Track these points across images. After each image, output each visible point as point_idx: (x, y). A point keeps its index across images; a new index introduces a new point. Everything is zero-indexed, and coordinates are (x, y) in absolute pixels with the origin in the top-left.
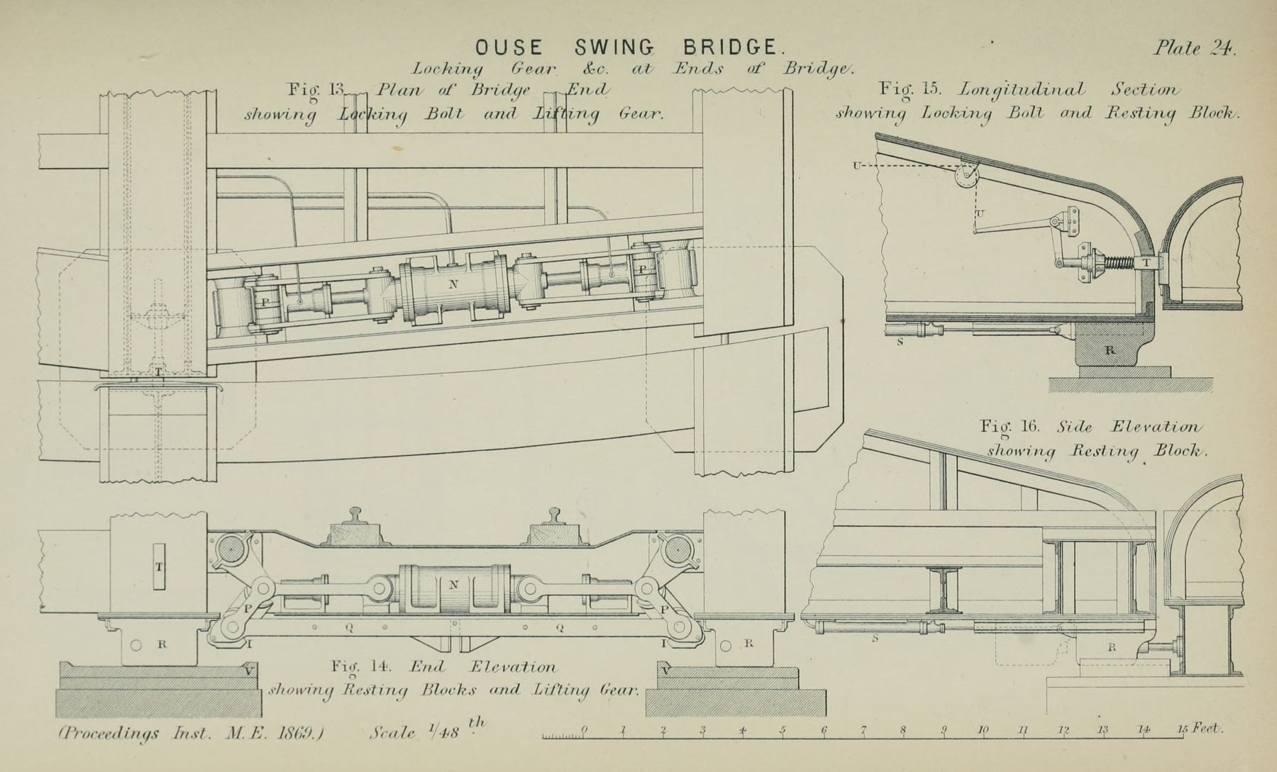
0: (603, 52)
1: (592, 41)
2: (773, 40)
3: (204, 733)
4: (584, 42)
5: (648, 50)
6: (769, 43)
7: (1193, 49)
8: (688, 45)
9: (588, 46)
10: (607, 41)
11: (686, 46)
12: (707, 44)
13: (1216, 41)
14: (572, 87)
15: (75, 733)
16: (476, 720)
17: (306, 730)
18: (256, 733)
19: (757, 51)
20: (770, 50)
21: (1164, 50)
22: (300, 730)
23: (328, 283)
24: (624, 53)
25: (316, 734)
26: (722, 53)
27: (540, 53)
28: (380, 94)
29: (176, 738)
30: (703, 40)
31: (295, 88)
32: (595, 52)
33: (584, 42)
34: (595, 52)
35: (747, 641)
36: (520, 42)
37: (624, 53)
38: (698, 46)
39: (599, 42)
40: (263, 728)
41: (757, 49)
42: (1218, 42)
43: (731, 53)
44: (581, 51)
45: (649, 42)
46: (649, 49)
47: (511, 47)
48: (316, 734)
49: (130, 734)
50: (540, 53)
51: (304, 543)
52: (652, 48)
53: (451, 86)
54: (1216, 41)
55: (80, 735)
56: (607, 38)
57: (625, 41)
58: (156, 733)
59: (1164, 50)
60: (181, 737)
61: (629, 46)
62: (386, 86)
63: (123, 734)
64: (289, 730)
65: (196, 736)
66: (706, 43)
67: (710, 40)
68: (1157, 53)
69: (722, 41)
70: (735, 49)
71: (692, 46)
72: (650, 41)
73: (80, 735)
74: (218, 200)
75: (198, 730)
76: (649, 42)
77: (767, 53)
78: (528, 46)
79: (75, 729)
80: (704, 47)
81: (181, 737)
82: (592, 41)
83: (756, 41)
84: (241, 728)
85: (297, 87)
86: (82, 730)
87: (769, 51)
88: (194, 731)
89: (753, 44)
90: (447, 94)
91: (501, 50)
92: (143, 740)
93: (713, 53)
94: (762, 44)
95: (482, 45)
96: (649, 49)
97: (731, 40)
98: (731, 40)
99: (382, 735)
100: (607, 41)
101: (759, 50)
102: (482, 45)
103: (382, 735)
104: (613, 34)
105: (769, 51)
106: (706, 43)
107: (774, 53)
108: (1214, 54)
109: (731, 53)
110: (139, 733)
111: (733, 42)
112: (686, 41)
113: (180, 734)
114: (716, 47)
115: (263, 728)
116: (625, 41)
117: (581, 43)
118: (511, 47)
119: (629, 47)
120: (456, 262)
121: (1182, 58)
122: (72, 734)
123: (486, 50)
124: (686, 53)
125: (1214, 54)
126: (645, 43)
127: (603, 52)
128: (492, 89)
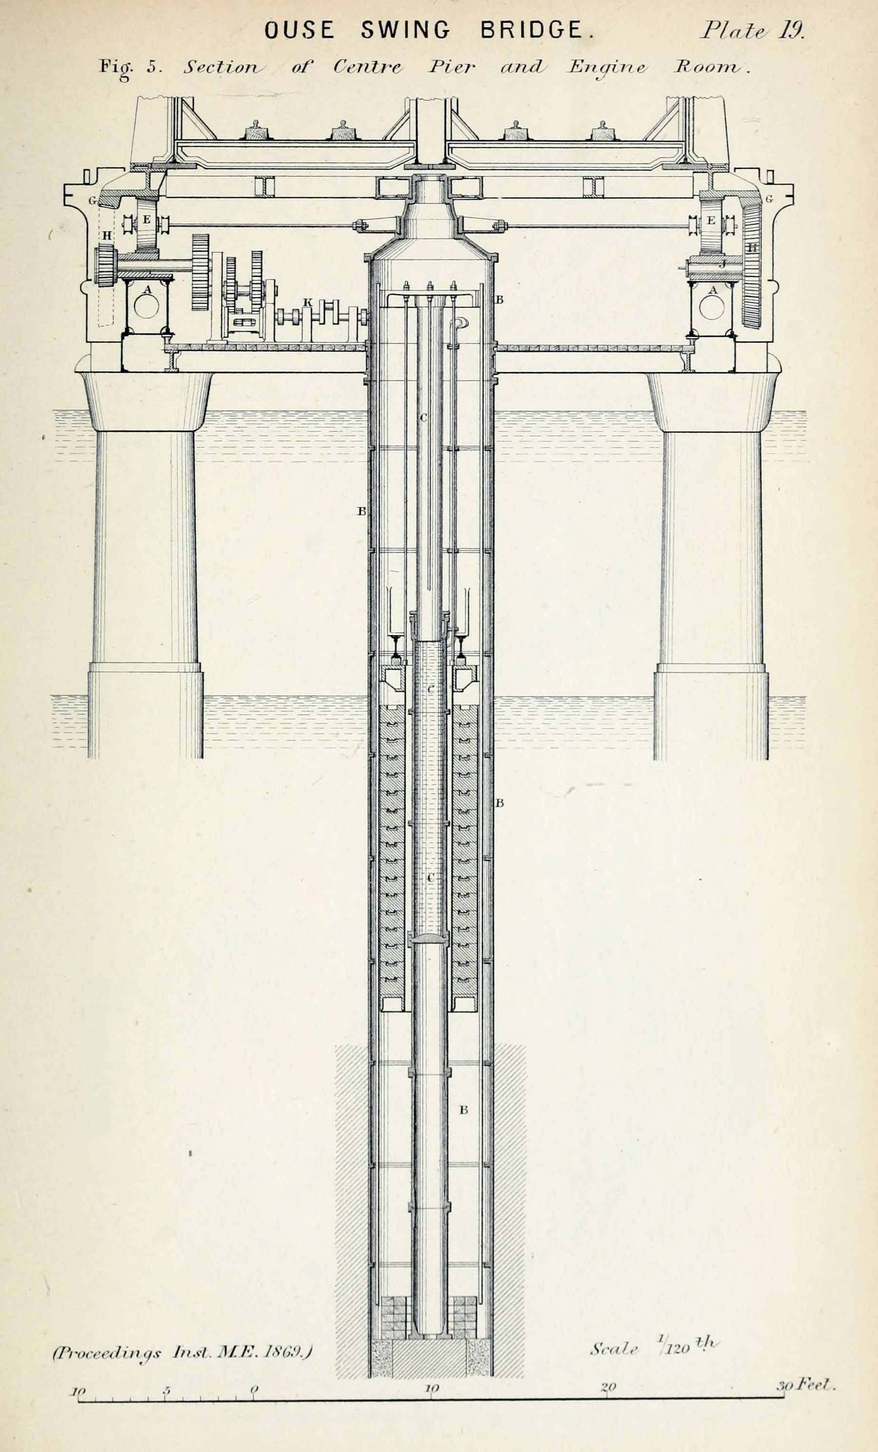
0: (393, 35)
1: (380, 22)
4: (371, 23)
5: (444, 33)
6: (574, 25)
8: (486, 27)
10: (397, 22)
11: (484, 28)
12: (506, 26)
14: (575, 64)
15: (70, 1353)
16: (704, 1339)
17: (294, 1349)
19: (561, 33)
20: (575, 33)
21: (714, 33)
22: (288, 1350)
23: (300, 322)
24: (416, 36)
28: (433, 71)
30: (502, 22)
32: (384, 36)
33: (313, 23)
34: (384, 36)
35: (462, 1107)
36: (369, 24)
37: (416, 36)
38: (497, 28)
39: (389, 24)
40: (253, 1347)
41: (561, 31)
43: (532, 36)
45: (446, 24)
46: (446, 32)
47: (301, 29)
48: (305, 1352)
49: (128, 1354)
52: (448, 31)
53: (307, 62)
55: (74, 1355)
57: (417, 23)
58: (158, 1353)
61: (421, 28)
62: (439, 63)
63: (121, 1353)
64: (276, 1349)
65: (279, 1353)
66: (505, 25)
67: (490, 22)
70: (537, 32)
71: (489, 29)
73: (74, 1355)
74: (775, 183)
75: (200, 1349)
76: (446, 24)
78: (318, 28)
79: (70, 1349)
80: (502, 29)
82: (380, 22)
83: (560, 24)
84: (235, 1347)
88: (156, 1351)
89: (556, 26)
91: (290, 32)
92: (144, 1360)
93: (512, 37)
94: (566, 27)
96: (446, 32)
97: (532, 22)
98: (532, 22)
99: (603, 1351)
100: (397, 22)
101: (563, 32)
103: (603, 1351)
104: (401, 15)
106: (505, 25)
107: (502, 37)
109: (532, 36)
112: (483, 22)
114: (517, 30)
115: (253, 1347)
116: (417, 23)
117: (309, 25)
119: (422, 29)
120: (239, 297)
122: (66, 1355)
123: (551, 24)
126: (441, 25)
127: (393, 35)
128: (391, 66)
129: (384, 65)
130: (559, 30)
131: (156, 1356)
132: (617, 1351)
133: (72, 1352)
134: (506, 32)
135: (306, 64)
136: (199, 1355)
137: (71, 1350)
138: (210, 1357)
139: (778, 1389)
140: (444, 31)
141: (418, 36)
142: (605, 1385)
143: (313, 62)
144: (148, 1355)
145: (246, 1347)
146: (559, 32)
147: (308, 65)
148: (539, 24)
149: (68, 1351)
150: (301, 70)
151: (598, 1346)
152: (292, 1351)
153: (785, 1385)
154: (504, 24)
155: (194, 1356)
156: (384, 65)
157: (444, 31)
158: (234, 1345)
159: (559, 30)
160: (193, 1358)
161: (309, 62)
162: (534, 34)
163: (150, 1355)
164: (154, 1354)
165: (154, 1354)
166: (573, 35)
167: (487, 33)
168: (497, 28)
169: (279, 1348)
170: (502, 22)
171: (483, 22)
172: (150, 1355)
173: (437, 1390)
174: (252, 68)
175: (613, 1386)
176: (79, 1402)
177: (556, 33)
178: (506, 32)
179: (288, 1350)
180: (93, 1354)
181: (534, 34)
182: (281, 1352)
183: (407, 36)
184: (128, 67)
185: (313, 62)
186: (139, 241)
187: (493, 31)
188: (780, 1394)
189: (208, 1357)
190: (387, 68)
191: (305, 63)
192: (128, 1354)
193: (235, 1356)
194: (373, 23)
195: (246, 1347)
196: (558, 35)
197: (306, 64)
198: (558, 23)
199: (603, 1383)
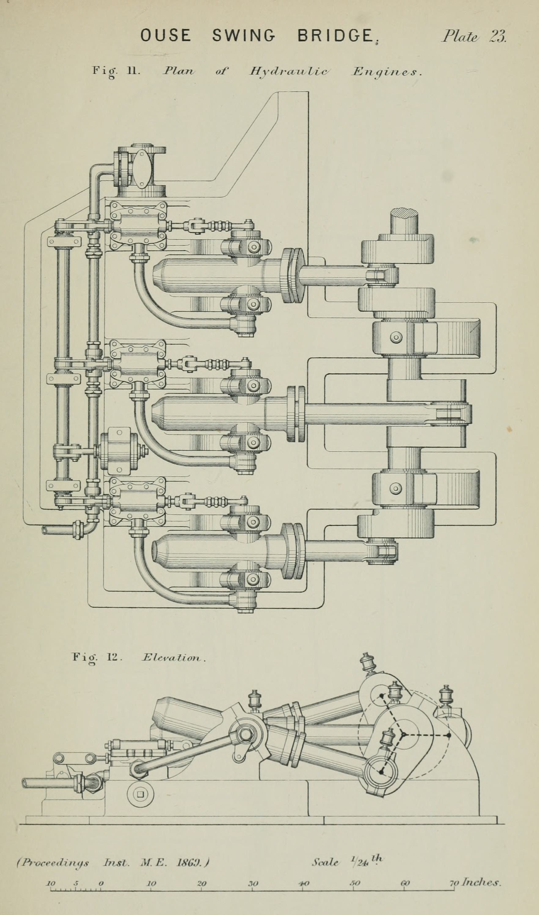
0: (236, 39)
2: (370, 30)
3: (125, 863)
4: (176, 30)
6: (367, 32)
7: (471, 38)
8: (302, 35)
9: (223, 34)
11: (300, 35)
12: (317, 33)
13: (493, 32)
15: (30, 863)
16: (376, 857)
18: (159, 863)
20: (186, 37)
21: (451, 38)
24: (251, 40)
25: (203, 862)
26: (328, 40)
27: (189, 40)
29: (106, 865)
30: (313, 30)
31: (97, 69)
32: (229, 39)
33: (220, 31)
34: (229, 39)
37: (251, 40)
38: (309, 35)
39: (233, 31)
40: (163, 859)
41: (357, 36)
42: (495, 32)
43: (336, 40)
44: (217, 38)
46: (272, 37)
47: (168, 34)
48: (203, 862)
50: (189, 40)
51: (267, 549)
52: (359, 36)
53: (225, 68)
54: (493, 32)
55: (34, 864)
56: (372, 30)
57: (252, 31)
59: (451, 38)
60: (109, 865)
63: (63, 863)
66: (315, 32)
68: (445, 41)
69: (328, 30)
72: (273, 30)
73: (34, 864)
76: (357, 32)
77: (365, 40)
78: (179, 34)
79: (30, 860)
80: (313, 35)
81: (109, 865)
83: (357, 32)
85: (98, 69)
86: (35, 861)
87: (366, 39)
88: (86, 862)
89: (354, 33)
90: (222, 74)
91: (160, 37)
92: (78, 867)
95: (146, 33)
98: (336, 30)
101: (359, 37)
102: (146, 33)
105: (366, 39)
106: (315, 32)
108: (493, 41)
110: (75, 862)
111: (338, 32)
112: (300, 30)
113: (108, 863)
114: (323, 36)
115: (163, 859)
116: (252, 31)
117: (174, 32)
118: (168, 34)
119: (256, 36)
121: (464, 44)
124: (300, 40)
125: (493, 41)
127: (236, 39)
128: (286, 71)
129: (282, 71)
130: (356, 36)
131: (86, 865)
132: (327, 864)
133: (31, 862)
134: (316, 38)
135: (224, 70)
136: (186, 864)
137: (31, 861)
138: (129, 866)
139: (249, 885)
140: (271, 36)
141: (253, 40)
142: (200, 882)
143: (228, 68)
144: (80, 864)
145: (159, 859)
146: (356, 37)
147: (225, 71)
148: (341, 32)
149: (28, 862)
150: (221, 73)
151: (317, 860)
152: (194, 863)
153: (253, 883)
154: (301, 31)
155: (117, 865)
156: (282, 71)
157: (271, 36)
158: (314, 860)
159: (356, 36)
160: (116, 866)
161: (226, 69)
162: (338, 39)
163: (82, 864)
164: (84, 863)
165: (84, 863)
166: (185, 39)
167: (303, 38)
168: (309, 35)
169: (186, 861)
170: (313, 30)
171: (300, 30)
172: (82, 864)
173: (54, 884)
174: (189, 72)
175: (154, 883)
176: (51, 891)
177: (354, 38)
178: (316, 38)
179: (192, 861)
180: (45, 864)
181: (338, 39)
182: (187, 863)
183: (245, 40)
184: (112, 71)
185: (228, 68)
186: (413, 240)
187: (306, 37)
188: (452, 888)
189: (127, 866)
190: (284, 72)
191: (223, 69)
192: (68, 863)
193: (200, 866)
194: (221, 31)
195: (159, 859)
196: (355, 39)
197: (224, 70)
198: (355, 31)
199: (199, 880)
